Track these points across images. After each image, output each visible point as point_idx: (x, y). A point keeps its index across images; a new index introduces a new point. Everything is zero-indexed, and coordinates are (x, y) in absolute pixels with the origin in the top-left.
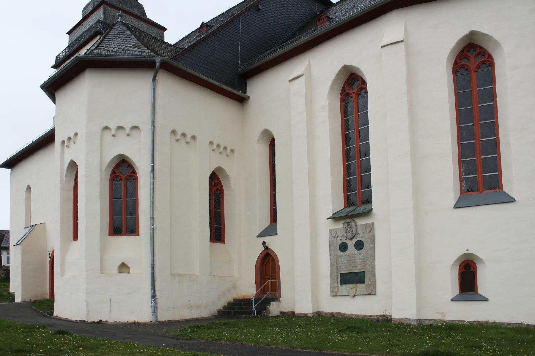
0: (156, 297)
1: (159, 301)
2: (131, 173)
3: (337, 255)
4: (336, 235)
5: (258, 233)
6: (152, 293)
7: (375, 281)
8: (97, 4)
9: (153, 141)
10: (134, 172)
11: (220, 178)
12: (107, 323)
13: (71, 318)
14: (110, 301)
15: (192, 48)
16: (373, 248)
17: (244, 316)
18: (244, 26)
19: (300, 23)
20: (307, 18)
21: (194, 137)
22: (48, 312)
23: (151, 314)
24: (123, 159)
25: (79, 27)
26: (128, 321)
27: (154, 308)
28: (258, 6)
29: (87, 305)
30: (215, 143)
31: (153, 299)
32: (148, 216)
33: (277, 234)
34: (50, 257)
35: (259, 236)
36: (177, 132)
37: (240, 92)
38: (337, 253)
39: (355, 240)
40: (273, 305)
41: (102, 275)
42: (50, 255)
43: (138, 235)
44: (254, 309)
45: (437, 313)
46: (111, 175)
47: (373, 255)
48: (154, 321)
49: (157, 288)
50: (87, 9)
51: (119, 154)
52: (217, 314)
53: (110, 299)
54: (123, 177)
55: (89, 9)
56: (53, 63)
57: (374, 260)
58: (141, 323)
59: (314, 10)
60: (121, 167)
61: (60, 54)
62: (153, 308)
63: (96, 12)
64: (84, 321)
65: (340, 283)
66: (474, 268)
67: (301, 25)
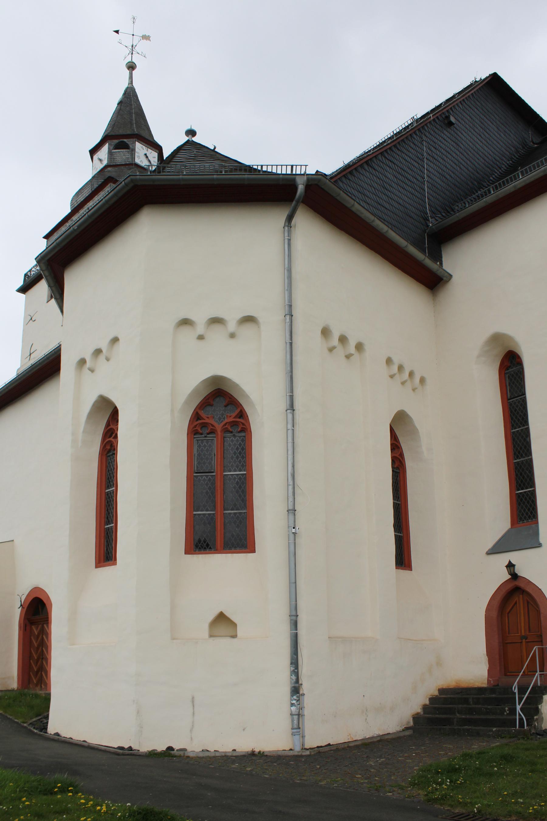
0: (301, 692)
1: (308, 701)
2: (235, 418)
6: (293, 682)
8: (97, 185)
10: (242, 414)
12: (186, 755)
13: (94, 739)
14: (193, 702)
15: (351, 173)
17: (494, 729)
18: (430, 149)
19: (510, 159)
20: (519, 152)
21: (359, 347)
22: (31, 722)
23: (290, 731)
24: (219, 389)
25: (65, 225)
26: (234, 750)
27: (297, 717)
28: (448, 117)
29: (138, 712)
30: (396, 360)
31: (295, 697)
32: (282, 508)
33: (540, 545)
34: (21, 605)
35: (495, 550)
36: (331, 331)
37: (438, 263)
41: (174, 641)
42: (21, 601)
43: (253, 551)
44: (519, 714)
46: (191, 422)
48: (298, 748)
49: (304, 670)
50: (80, 196)
51: (212, 376)
52: (412, 724)
53: (193, 698)
54: (219, 427)
55: (84, 195)
56: (20, 283)
58: (269, 754)
59: (527, 141)
60: (212, 405)
61: (32, 268)
62: (296, 717)
63: (96, 196)
64: (130, 748)
67: (511, 162)
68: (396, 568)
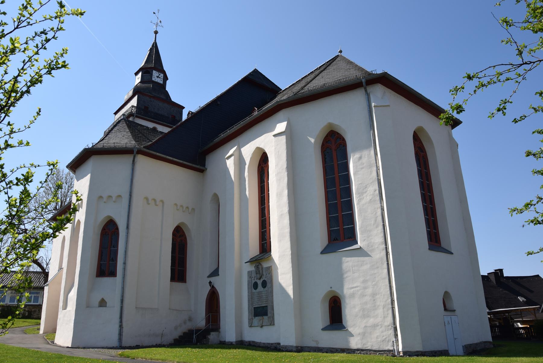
3: (252, 292)
4: (251, 276)
5: (208, 274)
7: (273, 314)
9: (130, 206)
11: (184, 231)
16: (272, 286)
33: (219, 275)
38: (252, 291)
39: (262, 280)
40: (213, 335)
45: (313, 341)
47: (272, 292)
57: (273, 296)
65: (254, 315)
66: (339, 303)
68: (171, 281)
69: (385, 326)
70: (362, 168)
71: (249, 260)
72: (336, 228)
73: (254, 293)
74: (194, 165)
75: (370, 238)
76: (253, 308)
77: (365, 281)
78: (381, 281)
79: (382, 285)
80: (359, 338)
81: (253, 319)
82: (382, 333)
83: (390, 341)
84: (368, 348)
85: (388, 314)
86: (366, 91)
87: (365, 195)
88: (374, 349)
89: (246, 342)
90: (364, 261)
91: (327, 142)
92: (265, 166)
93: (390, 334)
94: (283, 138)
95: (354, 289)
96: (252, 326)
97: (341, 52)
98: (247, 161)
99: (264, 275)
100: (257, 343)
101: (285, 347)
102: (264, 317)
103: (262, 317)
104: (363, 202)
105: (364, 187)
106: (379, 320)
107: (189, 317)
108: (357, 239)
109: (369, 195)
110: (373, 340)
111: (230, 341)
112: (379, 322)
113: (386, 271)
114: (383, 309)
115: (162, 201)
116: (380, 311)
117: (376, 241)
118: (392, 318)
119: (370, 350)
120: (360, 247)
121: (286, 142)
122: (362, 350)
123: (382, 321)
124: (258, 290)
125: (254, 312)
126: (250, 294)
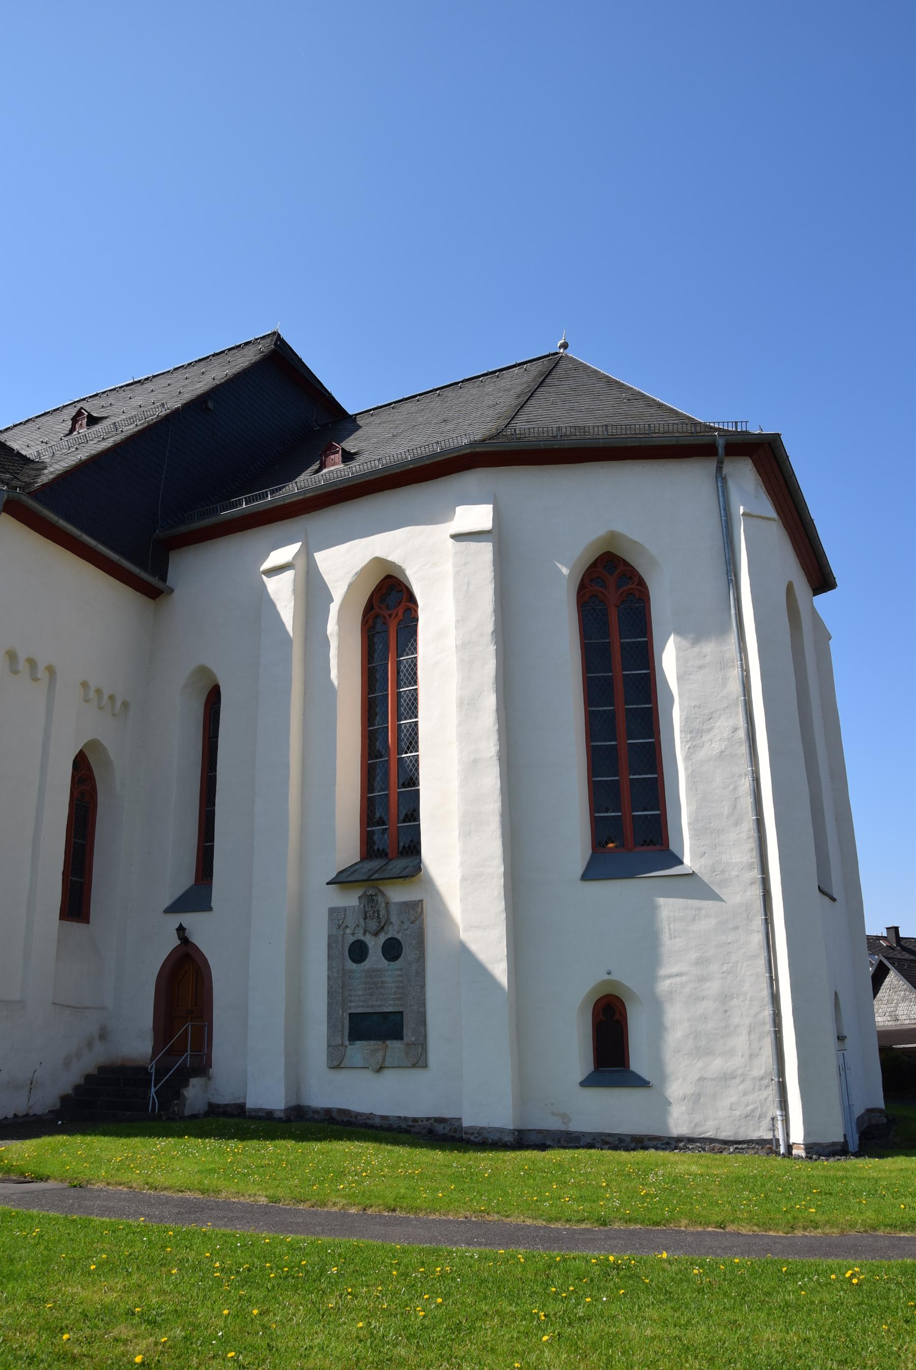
4: (342, 923)
17: (128, 1113)
35: (173, 909)
38: (343, 965)
39: (383, 938)
40: (194, 1086)
45: (553, 1114)
65: (349, 1036)
68: (60, 919)
69: (754, 1079)
70: (700, 667)
71: (334, 875)
72: (613, 814)
73: (351, 971)
74: (144, 576)
75: (718, 849)
76: (346, 1016)
77: (701, 962)
78: (745, 964)
79: (748, 973)
80: (684, 1108)
81: (346, 1047)
82: (744, 1095)
83: (765, 1117)
84: (707, 1135)
85: (760, 1048)
86: (719, 469)
87: (706, 738)
88: (722, 1138)
89: (316, 1111)
90: (700, 909)
91: (591, 580)
92: (390, 616)
93: (766, 1099)
94: (485, 551)
95: (674, 980)
96: (342, 1065)
97: (565, 346)
98: (338, 591)
99: (391, 923)
100: (358, 1114)
101: (478, 1133)
102: (388, 1042)
103: (380, 1043)
104: (702, 754)
105: (704, 715)
106: (736, 1062)
107: (101, 1029)
108: (672, 847)
109: (718, 739)
110: (720, 1114)
111: (264, 1107)
112: (737, 1068)
113: (758, 938)
114: (749, 1035)
115: (51, 670)
116: (740, 1041)
117: (734, 861)
118: (771, 1060)
119: (712, 1140)
120: (693, 872)
121: (494, 559)
122: (691, 1140)
123: (745, 1066)
124: (367, 964)
125: (350, 1027)
126: (335, 974)
